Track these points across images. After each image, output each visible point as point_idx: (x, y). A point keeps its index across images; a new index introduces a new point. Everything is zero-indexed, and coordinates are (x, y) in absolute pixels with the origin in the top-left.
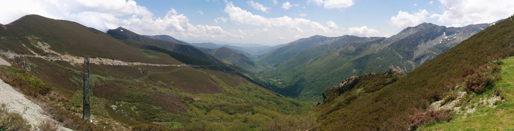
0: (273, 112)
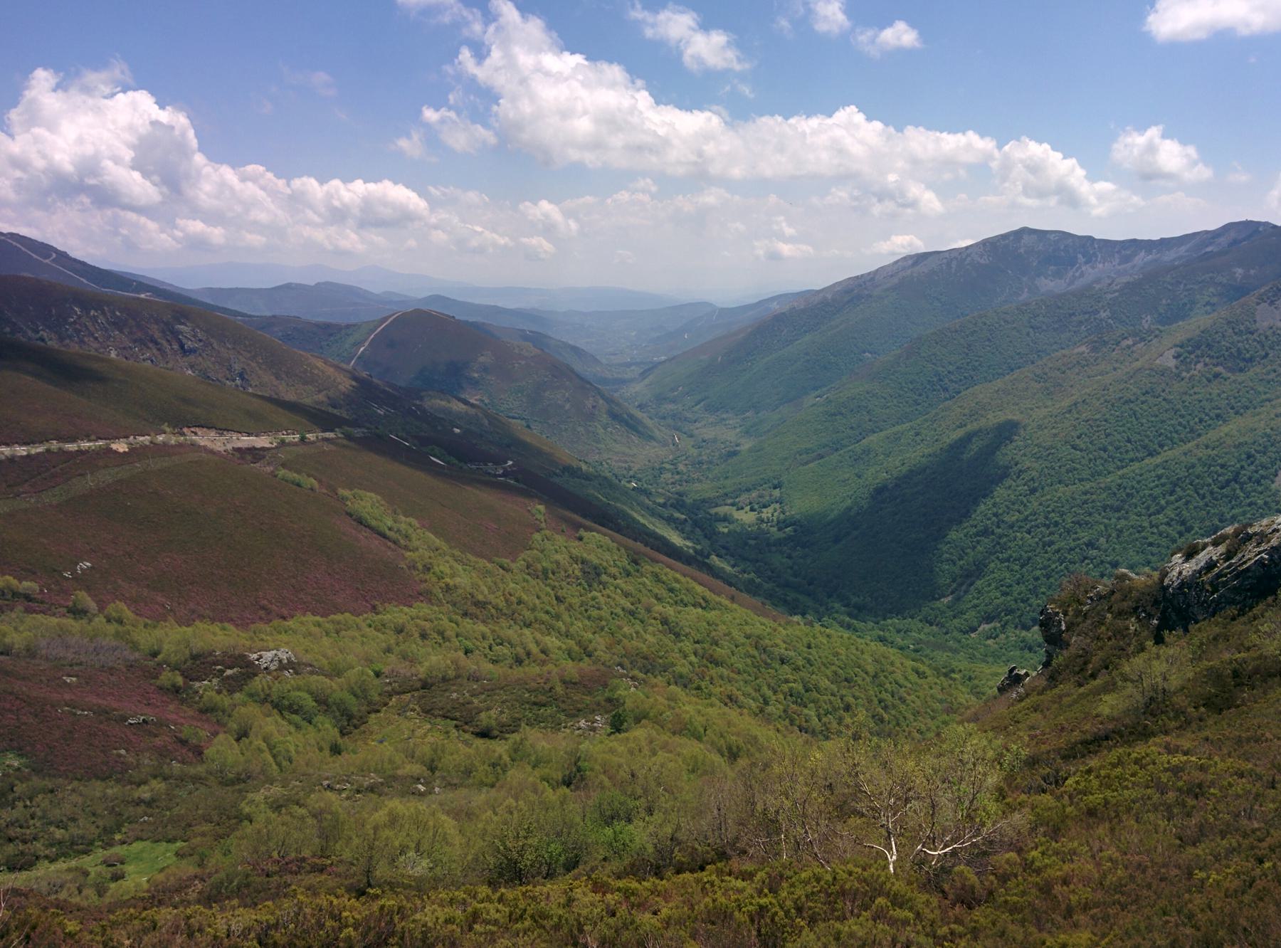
0: (733, 714)
